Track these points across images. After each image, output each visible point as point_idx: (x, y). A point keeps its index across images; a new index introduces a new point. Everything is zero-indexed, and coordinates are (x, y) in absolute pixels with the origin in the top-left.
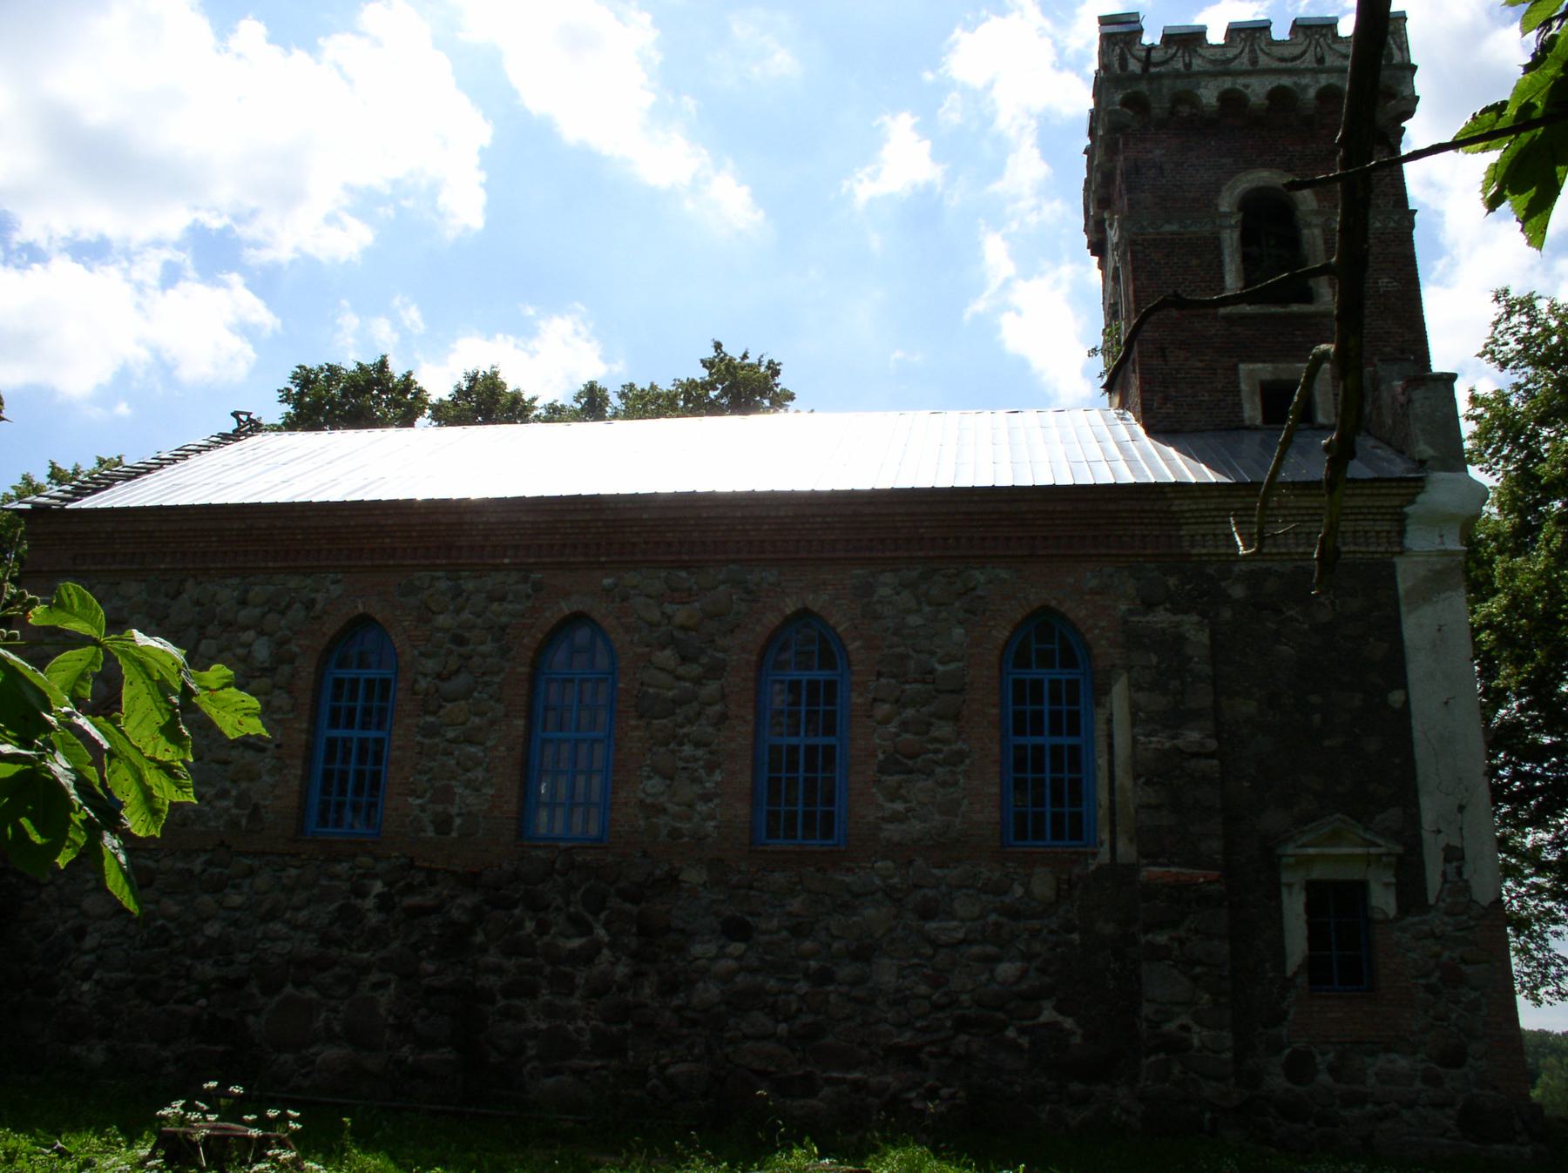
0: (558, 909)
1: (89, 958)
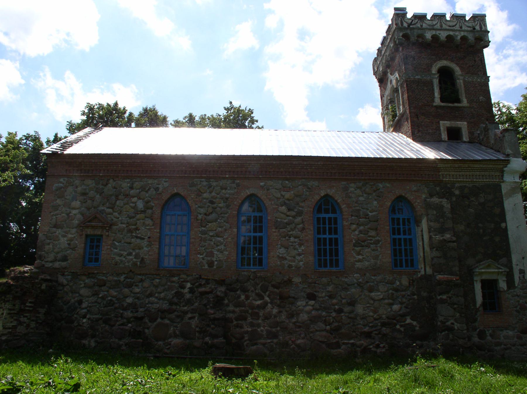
0: (252, 291)
1: (85, 310)
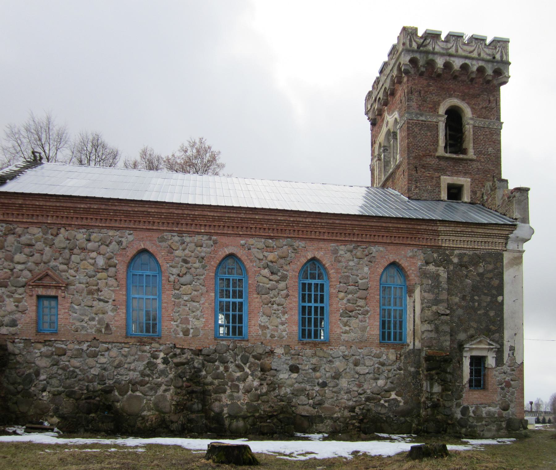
0: (232, 362)
